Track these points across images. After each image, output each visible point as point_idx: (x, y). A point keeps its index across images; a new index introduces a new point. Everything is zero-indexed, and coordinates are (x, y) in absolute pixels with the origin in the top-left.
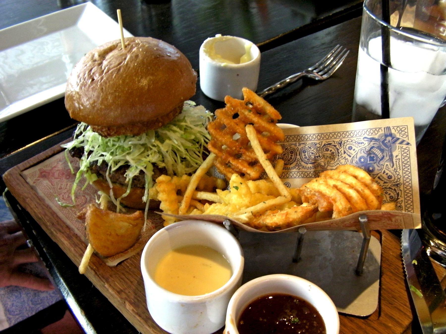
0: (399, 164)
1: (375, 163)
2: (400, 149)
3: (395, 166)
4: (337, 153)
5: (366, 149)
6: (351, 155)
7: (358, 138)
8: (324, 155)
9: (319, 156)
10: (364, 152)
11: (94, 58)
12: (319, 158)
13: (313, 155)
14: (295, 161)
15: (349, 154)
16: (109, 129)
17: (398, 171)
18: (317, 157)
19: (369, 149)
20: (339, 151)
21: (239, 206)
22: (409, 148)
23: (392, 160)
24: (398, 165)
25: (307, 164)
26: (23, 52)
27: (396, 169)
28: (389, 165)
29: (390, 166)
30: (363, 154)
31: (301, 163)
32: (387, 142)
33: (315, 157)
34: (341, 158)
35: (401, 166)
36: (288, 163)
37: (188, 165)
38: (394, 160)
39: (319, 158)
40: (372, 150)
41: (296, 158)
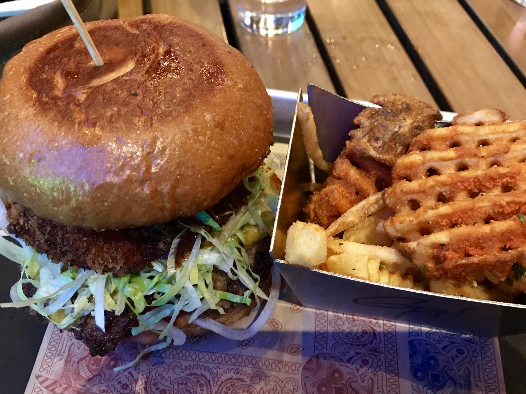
0: (63, 347)
1: (428, 382)
2: (51, 370)
3: (69, 344)
4: (149, 383)
5: (100, 381)
6: (128, 375)
7: (481, 367)
8: (171, 385)
9: (179, 384)
10: (105, 376)
11: (215, 119)
12: (180, 382)
13: (188, 388)
14: (222, 383)
15: (131, 378)
16: (77, 156)
17: (68, 337)
18: (182, 384)
19: (452, 376)
20: (144, 385)
21: (192, 126)
22: (298, 374)
23: (68, 354)
24: (64, 345)
25: (202, 375)
26: (49, 43)
27: (69, 340)
28: (76, 348)
29: (75, 346)
30: (346, 377)
31: (212, 377)
32: (64, 384)
33: (186, 384)
34: (145, 373)
35: (61, 345)
36: (236, 381)
37: (128, 127)
38: (66, 354)
39: (180, 382)
40: (91, 376)
41: (219, 388)
